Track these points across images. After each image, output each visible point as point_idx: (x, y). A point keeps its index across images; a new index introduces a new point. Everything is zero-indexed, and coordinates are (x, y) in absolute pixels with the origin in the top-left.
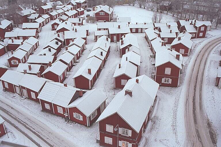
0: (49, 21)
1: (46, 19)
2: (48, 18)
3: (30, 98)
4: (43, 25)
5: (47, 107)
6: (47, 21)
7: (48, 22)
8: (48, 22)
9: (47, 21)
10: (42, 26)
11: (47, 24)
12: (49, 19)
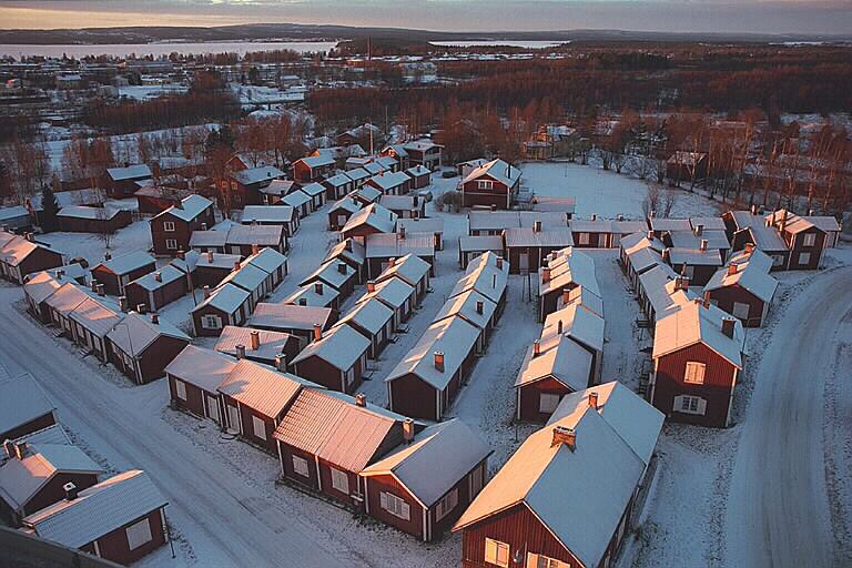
1: (313, 196)
3: (248, 435)
4: (305, 215)
5: (300, 466)
6: (317, 203)
7: (319, 206)
8: (319, 206)
9: (317, 203)
10: (302, 218)
11: (315, 210)
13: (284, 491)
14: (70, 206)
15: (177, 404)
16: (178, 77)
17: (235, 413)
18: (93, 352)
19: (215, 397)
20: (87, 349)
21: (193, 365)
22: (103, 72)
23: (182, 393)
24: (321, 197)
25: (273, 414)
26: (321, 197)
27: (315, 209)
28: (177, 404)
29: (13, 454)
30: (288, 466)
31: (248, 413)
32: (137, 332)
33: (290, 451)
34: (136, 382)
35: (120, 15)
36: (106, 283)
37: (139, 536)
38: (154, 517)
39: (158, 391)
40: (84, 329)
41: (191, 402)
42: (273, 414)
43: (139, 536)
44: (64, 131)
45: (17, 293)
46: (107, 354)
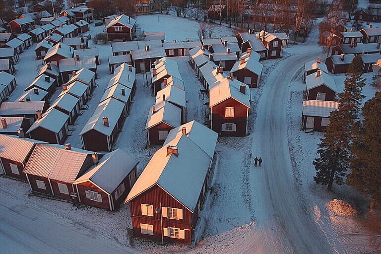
0: (31, 44)
1: (25, 41)
2: (28, 40)
4: (21, 52)
6: (27, 44)
7: (28, 46)
8: (28, 46)
9: (27, 44)
10: (20, 53)
12: (30, 40)
24: (29, 41)
26: (29, 41)
27: (27, 48)
42: (21, 160)
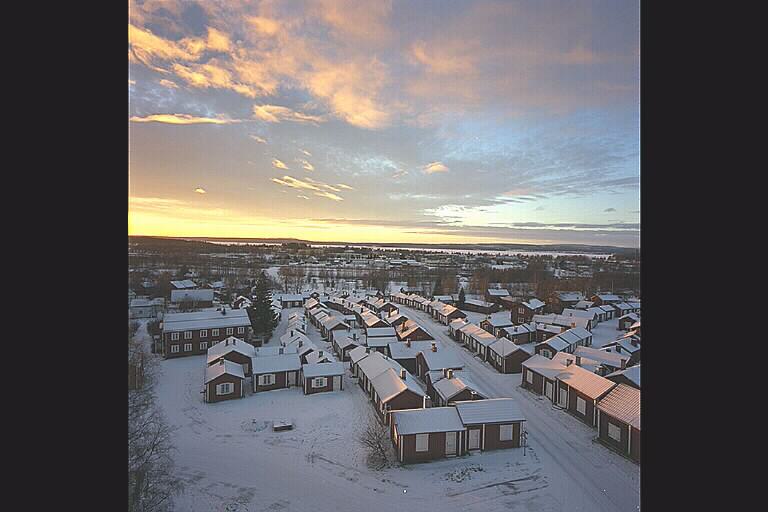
3: (572, 409)
5: (614, 432)
13: (599, 446)
14: (469, 300)
15: (526, 385)
16: (521, 263)
17: (564, 394)
18: (480, 355)
19: (551, 382)
20: (475, 354)
21: (537, 363)
22: (485, 259)
23: (530, 379)
25: (595, 396)
28: (526, 385)
29: (446, 376)
30: (604, 431)
31: (574, 393)
32: (505, 348)
33: (607, 419)
34: (501, 372)
35: (535, 240)
36: (490, 329)
37: (506, 433)
38: (516, 425)
39: (518, 378)
40: (477, 342)
41: (536, 385)
42: (595, 396)
43: (506, 433)
44: (466, 279)
45: (447, 328)
46: (488, 357)
